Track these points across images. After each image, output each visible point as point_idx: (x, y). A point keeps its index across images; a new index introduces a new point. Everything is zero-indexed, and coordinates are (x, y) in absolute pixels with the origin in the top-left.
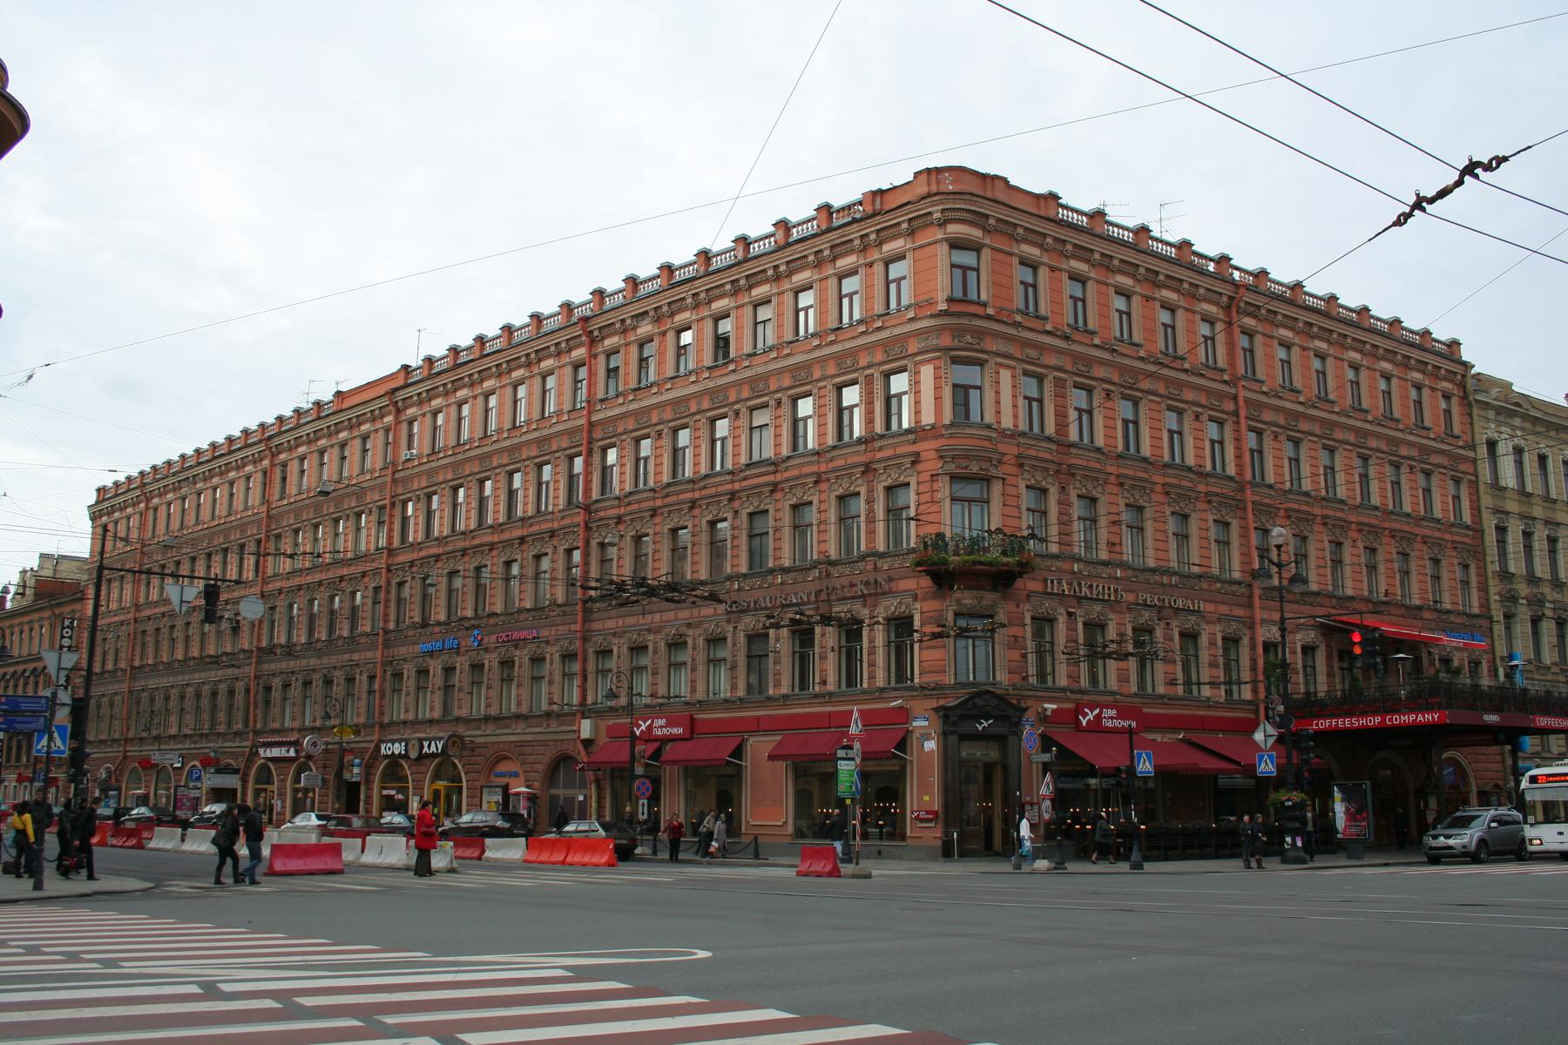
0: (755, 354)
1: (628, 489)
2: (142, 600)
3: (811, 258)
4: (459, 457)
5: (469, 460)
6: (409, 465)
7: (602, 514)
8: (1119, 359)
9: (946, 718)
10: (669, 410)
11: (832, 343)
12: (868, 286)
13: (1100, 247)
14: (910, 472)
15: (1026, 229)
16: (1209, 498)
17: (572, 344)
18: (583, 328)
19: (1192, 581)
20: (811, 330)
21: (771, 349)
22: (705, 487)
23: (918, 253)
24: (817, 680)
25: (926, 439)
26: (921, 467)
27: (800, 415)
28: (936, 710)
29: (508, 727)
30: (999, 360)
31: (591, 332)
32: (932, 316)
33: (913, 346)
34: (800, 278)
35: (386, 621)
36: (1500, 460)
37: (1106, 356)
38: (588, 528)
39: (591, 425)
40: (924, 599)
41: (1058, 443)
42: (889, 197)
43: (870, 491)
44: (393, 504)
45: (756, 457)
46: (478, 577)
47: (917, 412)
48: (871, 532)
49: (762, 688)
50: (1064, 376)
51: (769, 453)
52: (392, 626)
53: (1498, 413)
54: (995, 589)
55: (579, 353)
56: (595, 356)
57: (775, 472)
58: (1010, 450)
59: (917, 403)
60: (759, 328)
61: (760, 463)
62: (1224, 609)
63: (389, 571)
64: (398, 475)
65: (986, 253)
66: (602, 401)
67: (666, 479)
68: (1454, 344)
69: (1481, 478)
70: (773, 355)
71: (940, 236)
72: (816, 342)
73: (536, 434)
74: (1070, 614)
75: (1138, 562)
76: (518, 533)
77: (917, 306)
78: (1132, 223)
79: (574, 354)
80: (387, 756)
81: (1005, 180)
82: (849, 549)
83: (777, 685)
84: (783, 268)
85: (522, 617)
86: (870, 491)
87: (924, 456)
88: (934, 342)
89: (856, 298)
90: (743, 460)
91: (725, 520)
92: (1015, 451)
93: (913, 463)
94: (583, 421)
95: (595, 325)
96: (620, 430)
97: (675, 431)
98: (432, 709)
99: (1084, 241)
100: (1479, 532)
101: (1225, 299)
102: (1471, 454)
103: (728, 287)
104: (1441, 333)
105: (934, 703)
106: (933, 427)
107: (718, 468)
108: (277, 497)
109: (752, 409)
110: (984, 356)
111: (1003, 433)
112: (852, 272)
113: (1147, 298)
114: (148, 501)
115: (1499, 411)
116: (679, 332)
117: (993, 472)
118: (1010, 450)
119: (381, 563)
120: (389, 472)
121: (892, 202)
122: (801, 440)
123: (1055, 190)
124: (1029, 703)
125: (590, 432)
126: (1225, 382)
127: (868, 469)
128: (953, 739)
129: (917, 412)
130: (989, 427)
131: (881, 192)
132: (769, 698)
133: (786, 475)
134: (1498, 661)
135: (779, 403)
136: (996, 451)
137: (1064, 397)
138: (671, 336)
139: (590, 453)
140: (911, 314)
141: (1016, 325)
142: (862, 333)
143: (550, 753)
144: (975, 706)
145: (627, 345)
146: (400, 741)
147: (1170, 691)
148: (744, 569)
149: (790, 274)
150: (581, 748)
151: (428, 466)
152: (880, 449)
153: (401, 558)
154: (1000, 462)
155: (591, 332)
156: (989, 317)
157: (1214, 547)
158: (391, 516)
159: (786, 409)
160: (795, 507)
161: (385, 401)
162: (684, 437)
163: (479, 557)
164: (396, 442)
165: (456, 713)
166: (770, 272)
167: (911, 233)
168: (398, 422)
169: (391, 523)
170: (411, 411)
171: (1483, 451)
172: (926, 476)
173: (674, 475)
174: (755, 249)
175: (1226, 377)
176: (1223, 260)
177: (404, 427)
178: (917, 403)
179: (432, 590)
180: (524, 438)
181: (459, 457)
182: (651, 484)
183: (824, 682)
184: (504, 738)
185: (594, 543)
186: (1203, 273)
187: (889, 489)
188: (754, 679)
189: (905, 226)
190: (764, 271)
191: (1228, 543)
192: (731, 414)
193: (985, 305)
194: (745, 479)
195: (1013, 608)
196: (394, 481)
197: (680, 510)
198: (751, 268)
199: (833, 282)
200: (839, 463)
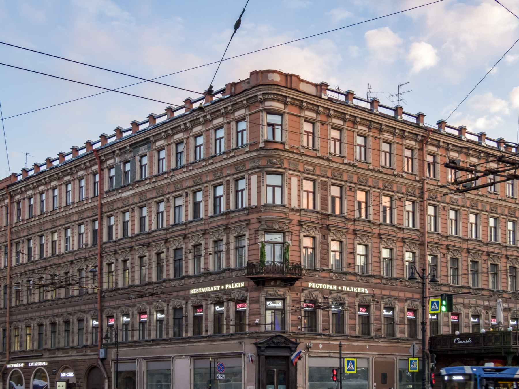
0: (159, 175)
1: (119, 238)
2: (14, 263)
3: (201, 119)
4: (42, 221)
5: (46, 222)
6: (18, 224)
7: (107, 250)
8: (357, 170)
9: (259, 348)
10: (138, 197)
11: (211, 164)
12: (228, 134)
14: (182, 243)
17: (92, 163)
19: (393, 281)
20: (223, 150)
21: (183, 167)
22: (137, 241)
23: (252, 116)
25: (253, 213)
26: (251, 227)
27: (240, 188)
29: (54, 354)
31: (100, 157)
32: (257, 150)
33: (249, 165)
34: (197, 129)
35: (10, 302)
37: (350, 168)
38: (101, 257)
39: (102, 205)
40: (251, 291)
41: (322, 214)
42: (238, 87)
43: (228, 238)
44: (11, 245)
45: (177, 222)
47: (249, 199)
48: (228, 259)
49: (199, 333)
50: (327, 180)
51: (183, 220)
54: (285, 286)
56: (103, 170)
57: (185, 229)
58: (295, 217)
59: (249, 194)
60: (148, 164)
61: (178, 225)
62: (409, 295)
63: (11, 278)
64: (13, 230)
65: (286, 116)
67: (137, 231)
70: (185, 170)
72: (204, 163)
73: (77, 210)
76: (70, 259)
77: (251, 145)
81: (298, 77)
82: (219, 267)
83: (187, 332)
84: (188, 124)
85: (73, 300)
86: (228, 238)
87: (252, 221)
88: (253, 165)
89: (223, 140)
90: (171, 222)
91: (163, 252)
92: (298, 218)
93: (247, 224)
95: (101, 154)
96: (115, 207)
97: (195, 193)
98: (87, 340)
99: (341, 108)
103: (163, 134)
105: (254, 341)
106: (256, 207)
107: (240, 207)
109: (175, 197)
110: (283, 171)
111: (292, 210)
112: (221, 127)
113: (375, 138)
114: (12, 197)
116: (159, 152)
118: (295, 217)
119: (7, 273)
120: (8, 228)
121: (239, 89)
122: (218, 208)
123: (325, 81)
124: (302, 340)
125: (101, 208)
127: (227, 228)
129: (249, 199)
131: (234, 84)
132: (183, 339)
133: (190, 230)
135: (187, 194)
136: (288, 219)
137: (326, 190)
138: (233, 124)
140: (247, 149)
141: (301, 154)
142: (225, 159)
143: (86, 366)
144: (273, 342)
145: (35, 194)
148: (172, 277)
150: (100, 362)
151: (27, 225)
152: (232, 218)
153: (16, 271)
154: (290, 223)
155: (100, 157)
159: (190, 198)
160: (215, 242)
162: (200, 197)
163: (79, 264)
165: (44, 347)
166: (183, 127)
167: (248, 107)
168: (12, 203)
170: (18, 197)
172: (252, 231)
173: (66, 250)
175: (418, 178)
177: (15, 205)
178: (249, 194)
179: (144, 268)
180: (57, 216)
181: (42, 221)
182: (165, 226)
184: (66, 358)
185: (104, 264)
187: (237, 237)
188: (177, 329)
190: (180, 126)
192: (130, 210)
194: (172, 232)
195: (294, 295)
196: (11, 233)
199: (173, 146)
200: (214, 224)
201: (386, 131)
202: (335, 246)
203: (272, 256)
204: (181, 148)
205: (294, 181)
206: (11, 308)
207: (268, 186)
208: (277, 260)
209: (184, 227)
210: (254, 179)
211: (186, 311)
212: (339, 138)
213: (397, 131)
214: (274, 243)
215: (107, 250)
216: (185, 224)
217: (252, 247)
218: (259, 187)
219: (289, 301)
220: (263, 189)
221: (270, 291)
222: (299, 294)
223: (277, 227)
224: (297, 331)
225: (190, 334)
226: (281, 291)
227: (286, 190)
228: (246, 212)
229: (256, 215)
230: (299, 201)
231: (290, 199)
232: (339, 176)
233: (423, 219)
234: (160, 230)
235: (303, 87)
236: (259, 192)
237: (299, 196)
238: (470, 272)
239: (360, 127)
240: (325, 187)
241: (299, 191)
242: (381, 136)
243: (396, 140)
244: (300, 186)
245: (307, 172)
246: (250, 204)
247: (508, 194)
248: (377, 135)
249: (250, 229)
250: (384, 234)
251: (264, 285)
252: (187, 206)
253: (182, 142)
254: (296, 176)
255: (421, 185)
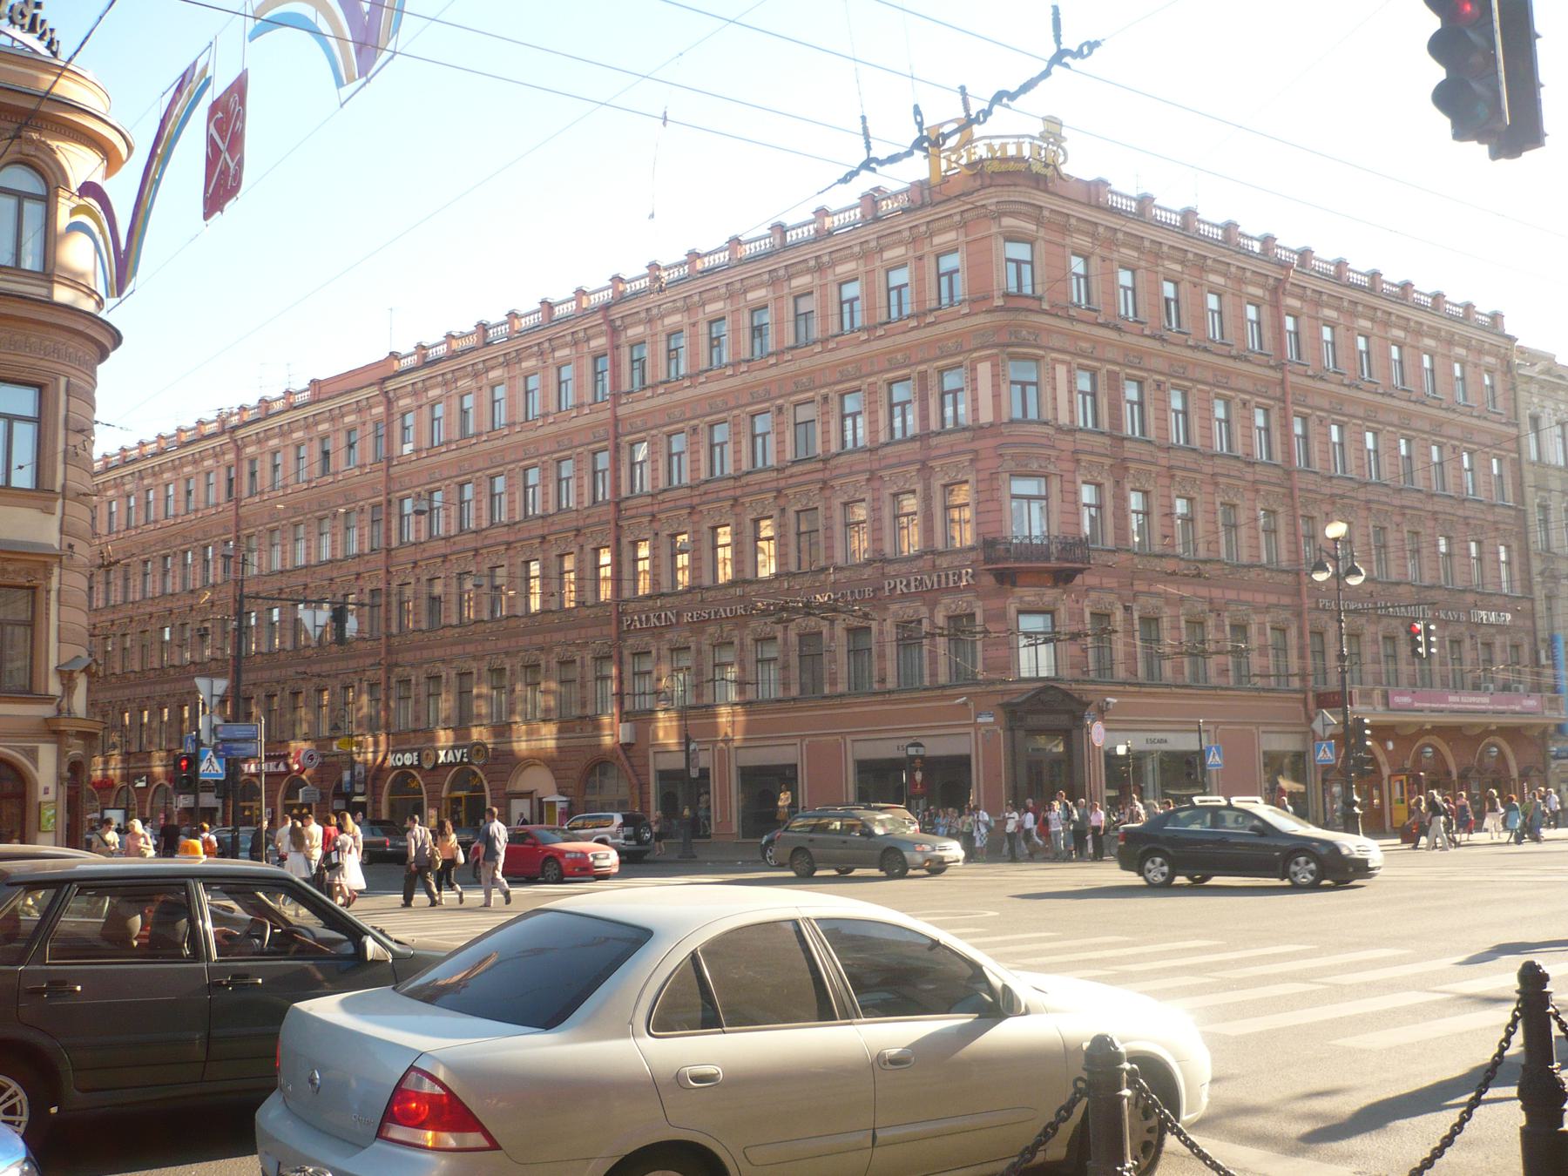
7: (629, 513)
8: (1169, 348)
13: (1149, 234)
15: (1079, 219)
16: (1255, 486)
18: (605, 317)
24: (876, 678)
25: (985, 437)
26: (980, 465)
28: (1003, 706)
30: (1054, 355)
32: (988, 311)
35: (388, 626)
36: (1545, 434)
45: (802, 456)
46: (492, 576)
49: (817, 681)
50: (1116, 368)
52: (394, 630)
53: (1542, 388)
55: (600, 342)
56: (617, 347)
62: (1272, 599)
65: (1040, 245)
66: (628, 393)
68: (1496, 318)
69: (1525, 456)
71: (994, 229)
74: (1126, 608)
75: (1190, 555)
77: (973, 301)
78: (1178, 207)
79: (593, 344)
80: (396, 768)
83: (833, 683)
94: (608, 414)
100: (1521, 514)
101: (1271, 281)
102: (1513, 431)
104: (1484, 307)
106: (992, 425)
108: (245, 493)
110: (1041, 352)
111: (1059, 429)
115: (1543, 385)
117: (1051, 468)
125: (616, 426)
126: (1271, 367)
128: (1020, 734)
130: (1046, 423)
134: (1540, 644)
139: (617, 448)
142: (913, 329)
146: (411, 751)
147: (1222, 682)
149: (833, 264)
156: (1045, 312)
157: (1262, 536)
158: (388, 514)
161: (374, 391)
164: (389, 435)
169: (389, 522)
171: (1526, 424)
174: (791, 237)
176: (1267, 241)
183: (883, 681)
186: (1249, 254)
189: (957, 218)
191: (1275, 531)
193: (1040, 299)
197: (719, 509)
198: (791, 258)
201: (1078, 231)
202: (1135, 501)
203: (1030, 523)
204: (805, 305)
205: (1061, 371)
206: (389, 636)
207: (1013, 382)
208: (1036, 532)
209: (820, 465)
210: (984, 369)
211: (832, 638)
212: (1028, 258)
213: (1101, 230)
214: (1029, 498)
215: (629, 513)
216: (825, 461)
217: (982, 508)
218: (996, 386)
219: (1062, 615)
220: (1004, 388)
221: (1028, 594)
222: (65, 547)
223: (1035, 466)
224: (1081, 677)
225: (842, 687)
226: (1050, 595)
227: (1047, 391)
228: (967, 434)
229: (990, 442)
230: (1071, 411)
231: (1055, 409)
232: (1032, 338)
233: (1115, 409)
234: (761, 471)
235: (1204, 229)
236: (996, 396)
237: (1071, 402)
238: (1221, 528)
239: (1123, 250)
240: (1115, 383)
241: (1070, 392)
242: (1115, 255)
243: (1042, 233)
244: (1071, 382)
245: (1082, 354)
246: (976, 419)
247: (1123, 312)
248: (1106, 253)
249: (978, 471)
250: (1133, 460)
251: (1014, 584)
252: (826, 423)
253: (811, 293)
254: (1063, 362)
255: (1279, 376)
